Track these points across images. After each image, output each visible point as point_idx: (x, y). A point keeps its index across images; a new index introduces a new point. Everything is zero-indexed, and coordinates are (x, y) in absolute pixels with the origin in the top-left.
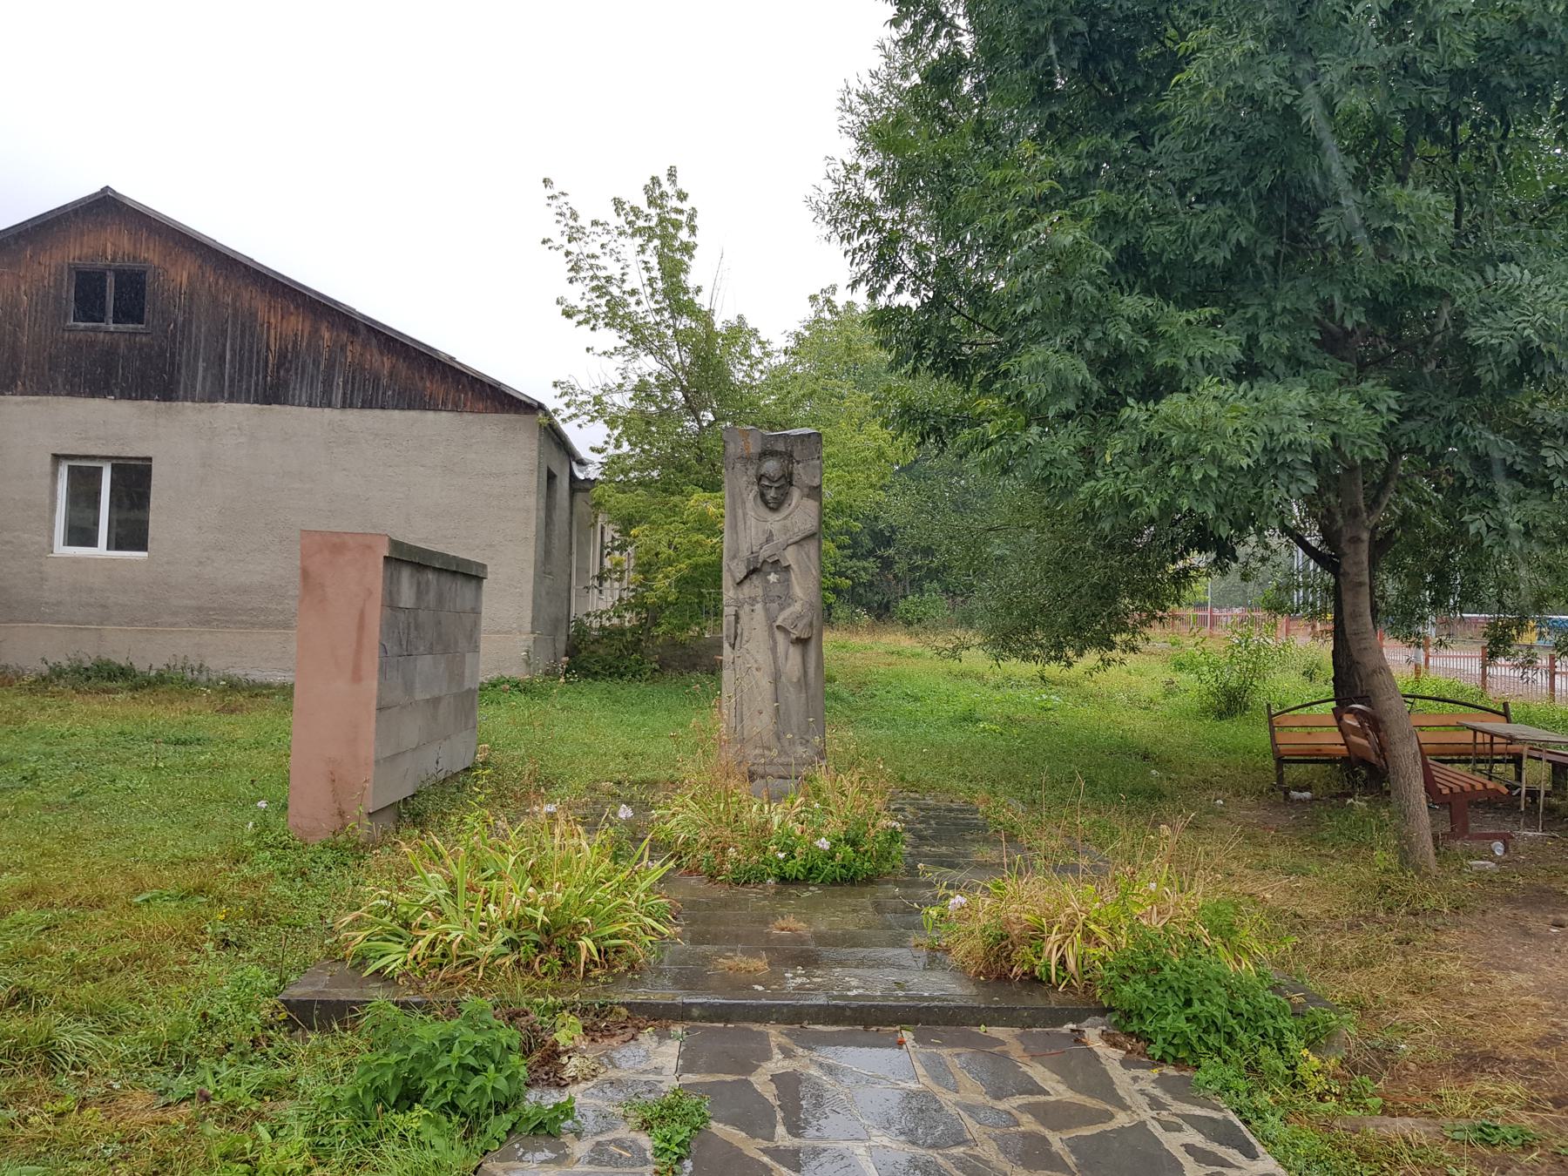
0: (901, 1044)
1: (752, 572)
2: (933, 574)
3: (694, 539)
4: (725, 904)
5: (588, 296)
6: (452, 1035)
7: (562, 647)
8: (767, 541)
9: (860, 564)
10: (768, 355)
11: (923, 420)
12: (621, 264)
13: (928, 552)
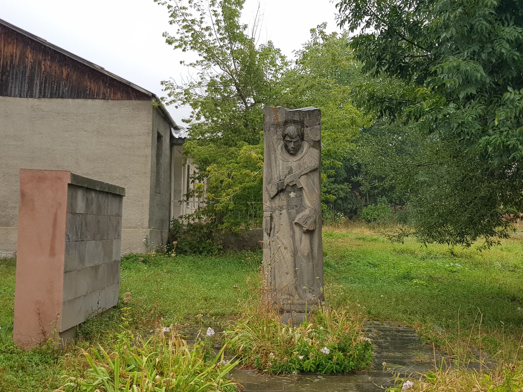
1: (281, 191)
2: (384, 192)
3: (244, 172)
5: (181, 31)
7: (166, 236)
9: (339, 186)
11: (382, 103)
12: (200, 13)
13: (381, 179)
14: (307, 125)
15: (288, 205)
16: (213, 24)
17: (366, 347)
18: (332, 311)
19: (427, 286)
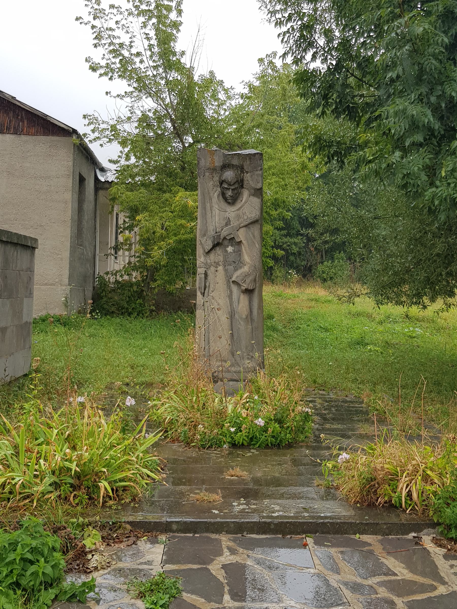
0: (305, 545)
1: (216, 245)
4: (196, 460)
6: (16, 540)
7: (89, 293)
8: (226, 225)
9: (292, 240)
10: (229, 98)
11: (330, 147)
12: (129, 35)
13: (335, 231)
14: (246, 170)
15: (225, 261)
16: (145, 50)
17: (306, 418)
18: (271, 379)
19: (382, 353)
